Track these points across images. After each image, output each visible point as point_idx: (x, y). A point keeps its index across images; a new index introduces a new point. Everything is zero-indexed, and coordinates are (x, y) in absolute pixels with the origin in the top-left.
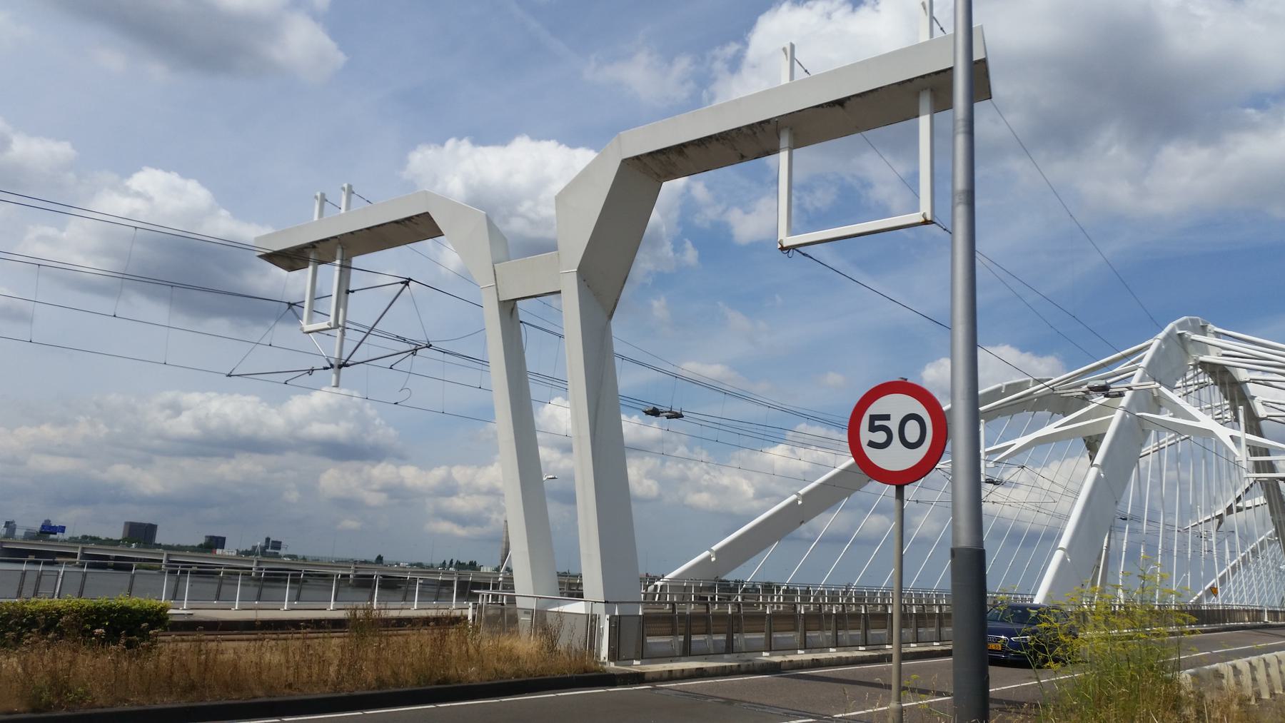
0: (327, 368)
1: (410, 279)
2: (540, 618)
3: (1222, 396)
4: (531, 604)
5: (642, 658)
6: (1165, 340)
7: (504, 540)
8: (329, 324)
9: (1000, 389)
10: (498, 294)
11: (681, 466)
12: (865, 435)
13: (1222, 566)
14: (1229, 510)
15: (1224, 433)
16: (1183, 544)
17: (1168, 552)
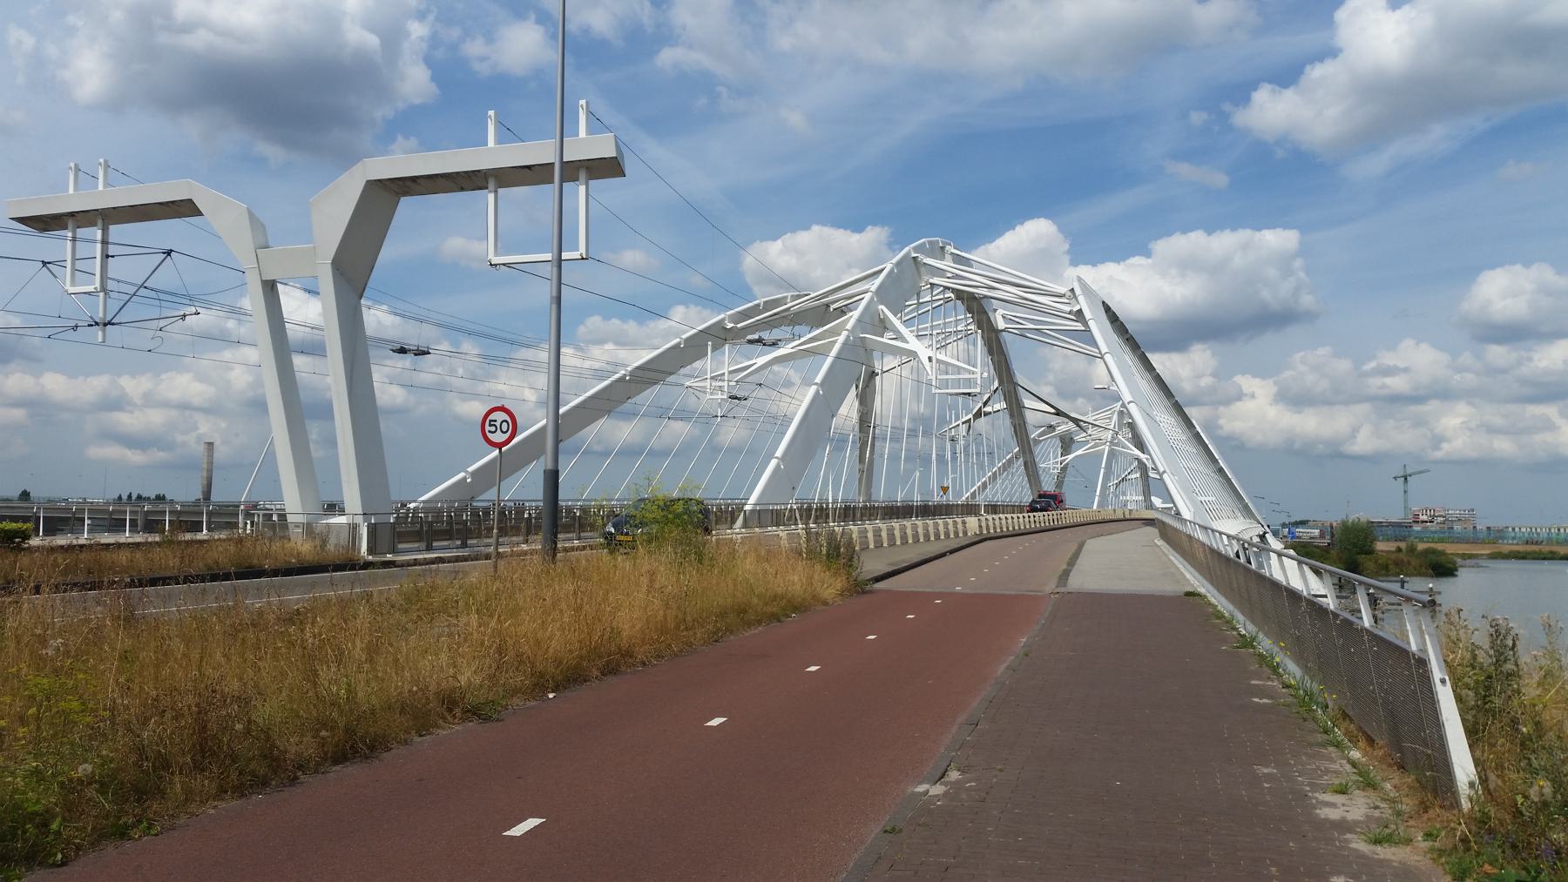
0: (92, 325)
1: (172, 251)
2: (309, 529)
4: (301, 519)
5: (394, 553)
6: (898, 264)
7: (205, 466)
8: (95, 288)
9: (758, 305)
10: (261, 275)
12: (487, 428)
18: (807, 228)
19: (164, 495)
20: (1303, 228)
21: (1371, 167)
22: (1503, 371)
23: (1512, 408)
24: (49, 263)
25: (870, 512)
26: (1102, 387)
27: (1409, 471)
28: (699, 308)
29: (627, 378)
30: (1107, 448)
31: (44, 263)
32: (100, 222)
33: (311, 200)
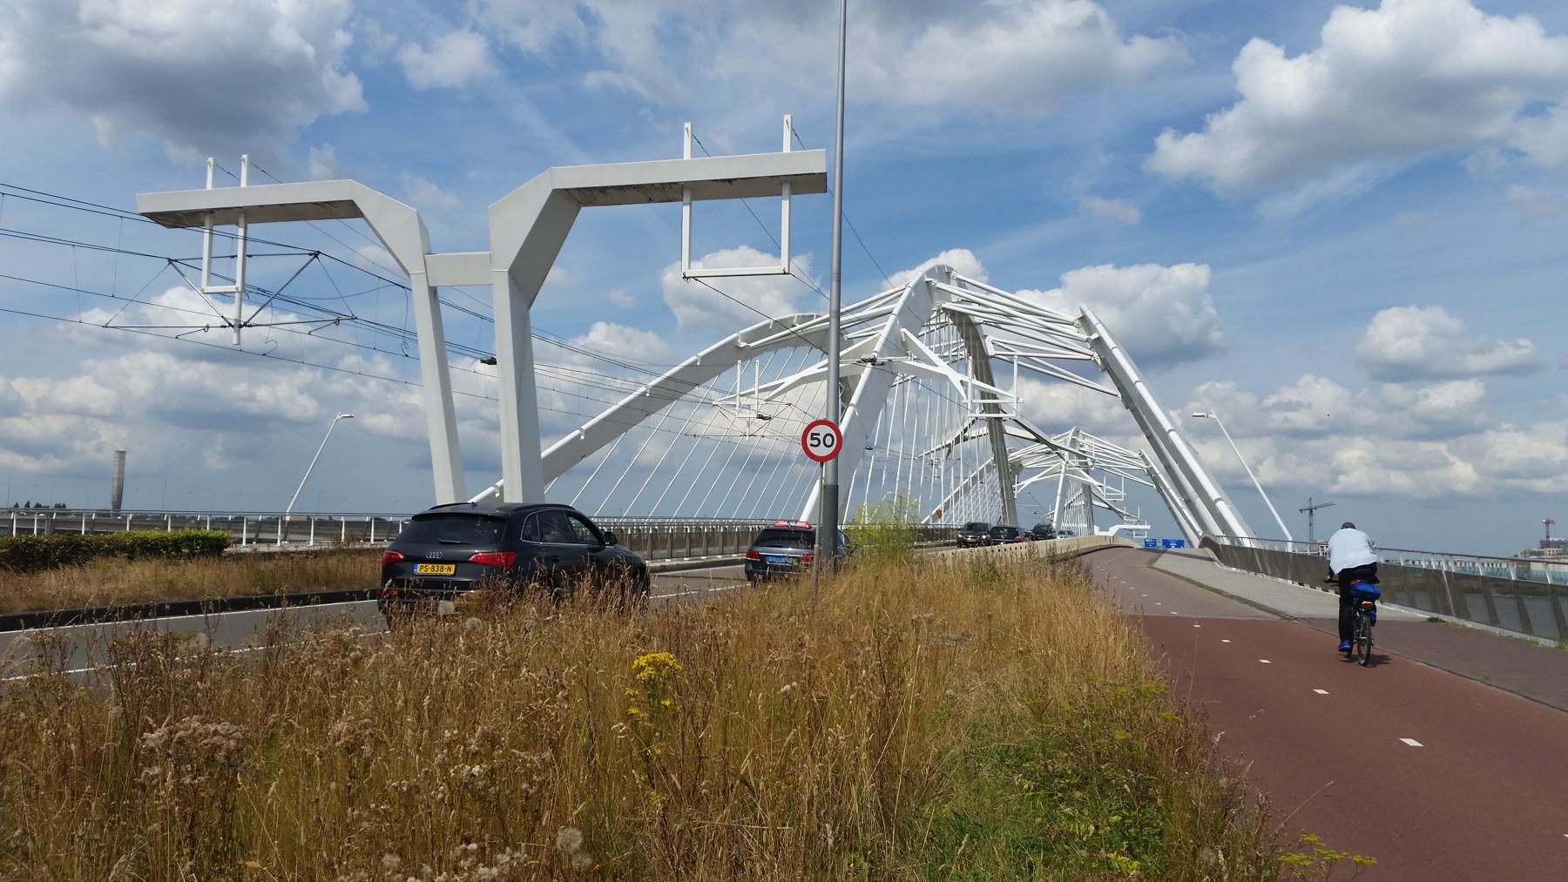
0: (225, 327)
3: (959, 335)
7: (116, 475)
10: (428, 281)
11: (350, 381)
12: (809, 441)
13: (947, 493)
14: (957, 440)
15: (955, 377)
16: (917, 471)
17: (904, 478)
18: (734, 247)
19: (64, 505)
20: (1215, 266)
21: (1285, 206)
22: (1402, 408)
23: (1408, 445)
24: (176, 261)
25: (1013, 535)
26: (1200, 414)
27: (1314, 504)
28: (620, 326)
29: (648, 395)
30: (1062, 475)
31: (170, 261)
32: (242, 220)
33: (490, 207)
